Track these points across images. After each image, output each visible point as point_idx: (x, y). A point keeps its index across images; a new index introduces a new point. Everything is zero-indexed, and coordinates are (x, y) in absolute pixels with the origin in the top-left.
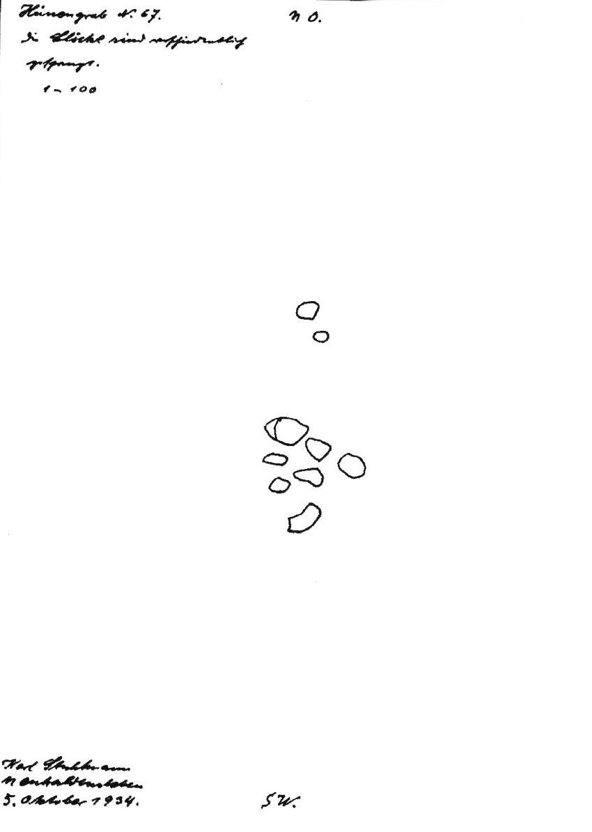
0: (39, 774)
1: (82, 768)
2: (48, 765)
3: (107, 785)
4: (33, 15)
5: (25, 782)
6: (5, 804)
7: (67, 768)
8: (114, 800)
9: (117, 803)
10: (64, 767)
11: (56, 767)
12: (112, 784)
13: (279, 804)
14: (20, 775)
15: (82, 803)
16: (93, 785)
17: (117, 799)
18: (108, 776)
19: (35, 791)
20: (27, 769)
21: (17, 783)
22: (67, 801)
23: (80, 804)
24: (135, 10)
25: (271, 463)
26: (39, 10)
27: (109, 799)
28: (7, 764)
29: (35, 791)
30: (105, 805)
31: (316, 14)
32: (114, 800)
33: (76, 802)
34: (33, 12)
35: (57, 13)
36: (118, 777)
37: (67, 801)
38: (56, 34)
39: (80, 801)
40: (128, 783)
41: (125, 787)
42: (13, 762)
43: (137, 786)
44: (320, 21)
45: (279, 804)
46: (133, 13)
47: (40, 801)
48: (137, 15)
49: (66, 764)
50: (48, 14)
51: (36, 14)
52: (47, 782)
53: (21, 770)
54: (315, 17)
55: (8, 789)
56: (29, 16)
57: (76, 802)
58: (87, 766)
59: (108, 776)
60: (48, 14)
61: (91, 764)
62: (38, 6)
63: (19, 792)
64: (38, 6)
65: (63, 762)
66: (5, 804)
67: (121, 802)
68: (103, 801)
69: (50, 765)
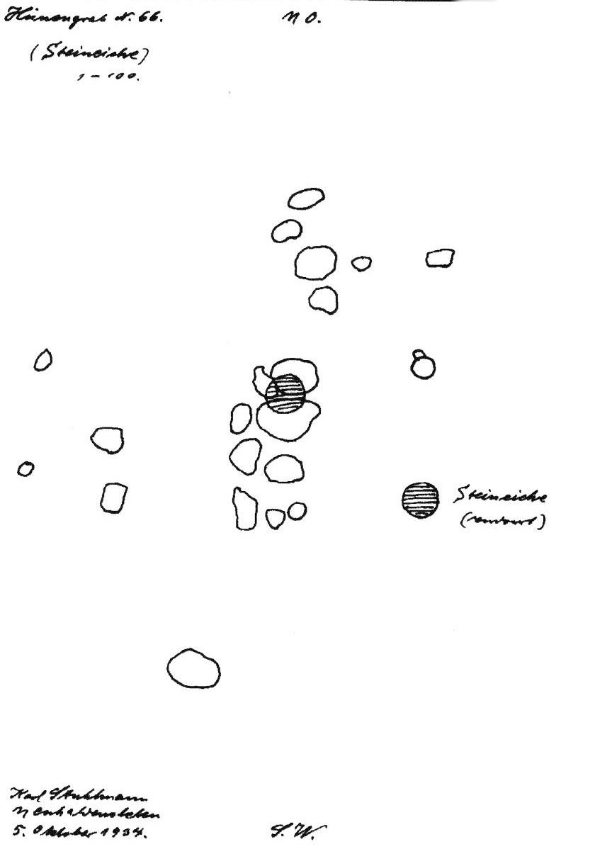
0: (46, 803)
1: (96, 797)
2: (55, 793)
3: (121, 815)
4: (23, 18)
5: (38, 811)
6: (14, 834)
7: (78, 797)
8: (121, 833)
9: (124, 835)
10: (74, 796)
11: (66, 795)
12: (125, 814)
13: (297, 834)
14: (31, 806)
15: (90, 834)
16: (106, 815)
17: (124, 831)
18: (118, 807)
19: (47, 822)
20: (36, 799)
21: (30, 813)
22: (77, 832)
23: (88, 836)
24: (133, 13)
25: (234, 496)
26: (31, 13)
27: (116, 831)
28: (15, 792)
29: (47, 822)
30: (113, 836)
31: (315, 14)
32: (121, 833)
33: (85, 834)
34: (21, 16)
35: (61, 20)
36: (134, 807)
37: (77, 832)
38: (98, 56)
39: (89, 833)
40: (82, 831)
41: (79, 836)
42: (20, 792)
43: (152, 816)
44: (319, 22)
45: (297, 834)
46: (131, 16)
47: (51, 832)
48: (135, 18)
49: (76, 792)
50: (42, 18)
51: (28, 17)
52: (60, 812)
53: (29, 800)
54: (313, 17)
55: (19, 819)
56: (18, 18)
57: (85, 834)
58: (100, 796)
59: (122, 805)
60: (42, 18)
61: (105, 794)
62: (31, 9)
63: (32, 821)
64: (31, 9)
65: (72, 791)
66: (14, 834)
67: (128, 833)
68: (110, 833)
69: (56, 794)
